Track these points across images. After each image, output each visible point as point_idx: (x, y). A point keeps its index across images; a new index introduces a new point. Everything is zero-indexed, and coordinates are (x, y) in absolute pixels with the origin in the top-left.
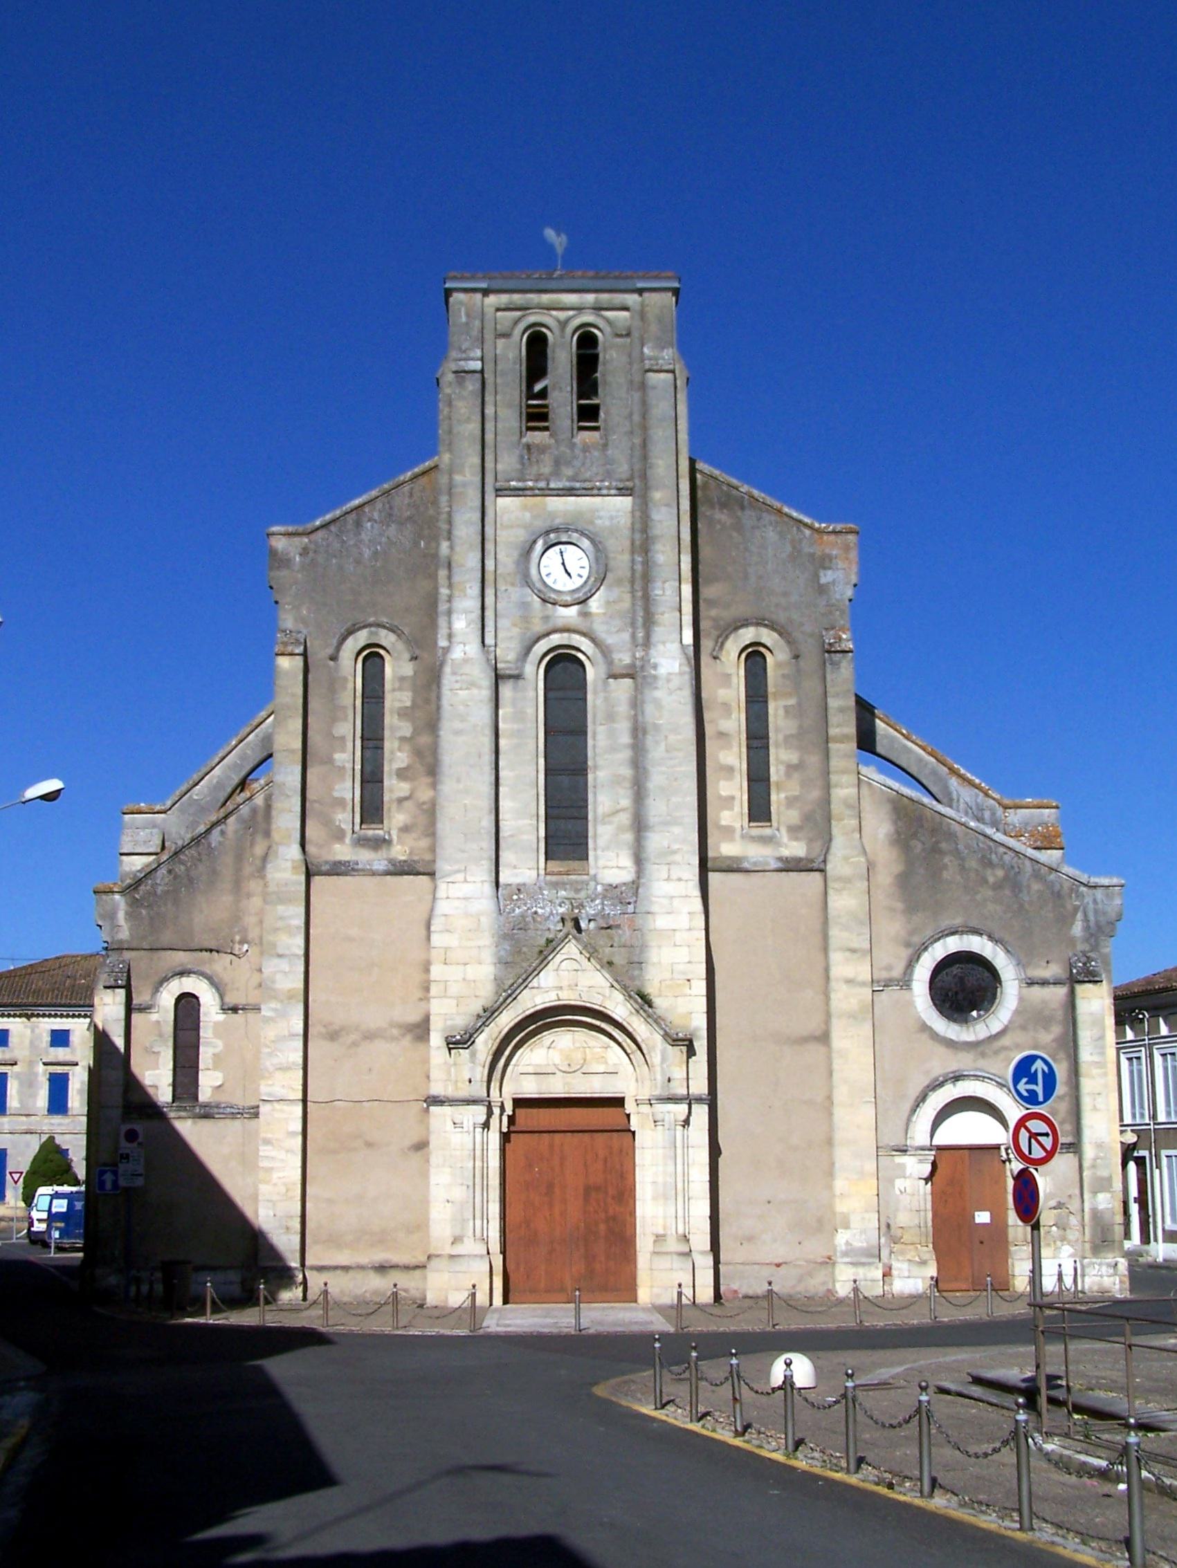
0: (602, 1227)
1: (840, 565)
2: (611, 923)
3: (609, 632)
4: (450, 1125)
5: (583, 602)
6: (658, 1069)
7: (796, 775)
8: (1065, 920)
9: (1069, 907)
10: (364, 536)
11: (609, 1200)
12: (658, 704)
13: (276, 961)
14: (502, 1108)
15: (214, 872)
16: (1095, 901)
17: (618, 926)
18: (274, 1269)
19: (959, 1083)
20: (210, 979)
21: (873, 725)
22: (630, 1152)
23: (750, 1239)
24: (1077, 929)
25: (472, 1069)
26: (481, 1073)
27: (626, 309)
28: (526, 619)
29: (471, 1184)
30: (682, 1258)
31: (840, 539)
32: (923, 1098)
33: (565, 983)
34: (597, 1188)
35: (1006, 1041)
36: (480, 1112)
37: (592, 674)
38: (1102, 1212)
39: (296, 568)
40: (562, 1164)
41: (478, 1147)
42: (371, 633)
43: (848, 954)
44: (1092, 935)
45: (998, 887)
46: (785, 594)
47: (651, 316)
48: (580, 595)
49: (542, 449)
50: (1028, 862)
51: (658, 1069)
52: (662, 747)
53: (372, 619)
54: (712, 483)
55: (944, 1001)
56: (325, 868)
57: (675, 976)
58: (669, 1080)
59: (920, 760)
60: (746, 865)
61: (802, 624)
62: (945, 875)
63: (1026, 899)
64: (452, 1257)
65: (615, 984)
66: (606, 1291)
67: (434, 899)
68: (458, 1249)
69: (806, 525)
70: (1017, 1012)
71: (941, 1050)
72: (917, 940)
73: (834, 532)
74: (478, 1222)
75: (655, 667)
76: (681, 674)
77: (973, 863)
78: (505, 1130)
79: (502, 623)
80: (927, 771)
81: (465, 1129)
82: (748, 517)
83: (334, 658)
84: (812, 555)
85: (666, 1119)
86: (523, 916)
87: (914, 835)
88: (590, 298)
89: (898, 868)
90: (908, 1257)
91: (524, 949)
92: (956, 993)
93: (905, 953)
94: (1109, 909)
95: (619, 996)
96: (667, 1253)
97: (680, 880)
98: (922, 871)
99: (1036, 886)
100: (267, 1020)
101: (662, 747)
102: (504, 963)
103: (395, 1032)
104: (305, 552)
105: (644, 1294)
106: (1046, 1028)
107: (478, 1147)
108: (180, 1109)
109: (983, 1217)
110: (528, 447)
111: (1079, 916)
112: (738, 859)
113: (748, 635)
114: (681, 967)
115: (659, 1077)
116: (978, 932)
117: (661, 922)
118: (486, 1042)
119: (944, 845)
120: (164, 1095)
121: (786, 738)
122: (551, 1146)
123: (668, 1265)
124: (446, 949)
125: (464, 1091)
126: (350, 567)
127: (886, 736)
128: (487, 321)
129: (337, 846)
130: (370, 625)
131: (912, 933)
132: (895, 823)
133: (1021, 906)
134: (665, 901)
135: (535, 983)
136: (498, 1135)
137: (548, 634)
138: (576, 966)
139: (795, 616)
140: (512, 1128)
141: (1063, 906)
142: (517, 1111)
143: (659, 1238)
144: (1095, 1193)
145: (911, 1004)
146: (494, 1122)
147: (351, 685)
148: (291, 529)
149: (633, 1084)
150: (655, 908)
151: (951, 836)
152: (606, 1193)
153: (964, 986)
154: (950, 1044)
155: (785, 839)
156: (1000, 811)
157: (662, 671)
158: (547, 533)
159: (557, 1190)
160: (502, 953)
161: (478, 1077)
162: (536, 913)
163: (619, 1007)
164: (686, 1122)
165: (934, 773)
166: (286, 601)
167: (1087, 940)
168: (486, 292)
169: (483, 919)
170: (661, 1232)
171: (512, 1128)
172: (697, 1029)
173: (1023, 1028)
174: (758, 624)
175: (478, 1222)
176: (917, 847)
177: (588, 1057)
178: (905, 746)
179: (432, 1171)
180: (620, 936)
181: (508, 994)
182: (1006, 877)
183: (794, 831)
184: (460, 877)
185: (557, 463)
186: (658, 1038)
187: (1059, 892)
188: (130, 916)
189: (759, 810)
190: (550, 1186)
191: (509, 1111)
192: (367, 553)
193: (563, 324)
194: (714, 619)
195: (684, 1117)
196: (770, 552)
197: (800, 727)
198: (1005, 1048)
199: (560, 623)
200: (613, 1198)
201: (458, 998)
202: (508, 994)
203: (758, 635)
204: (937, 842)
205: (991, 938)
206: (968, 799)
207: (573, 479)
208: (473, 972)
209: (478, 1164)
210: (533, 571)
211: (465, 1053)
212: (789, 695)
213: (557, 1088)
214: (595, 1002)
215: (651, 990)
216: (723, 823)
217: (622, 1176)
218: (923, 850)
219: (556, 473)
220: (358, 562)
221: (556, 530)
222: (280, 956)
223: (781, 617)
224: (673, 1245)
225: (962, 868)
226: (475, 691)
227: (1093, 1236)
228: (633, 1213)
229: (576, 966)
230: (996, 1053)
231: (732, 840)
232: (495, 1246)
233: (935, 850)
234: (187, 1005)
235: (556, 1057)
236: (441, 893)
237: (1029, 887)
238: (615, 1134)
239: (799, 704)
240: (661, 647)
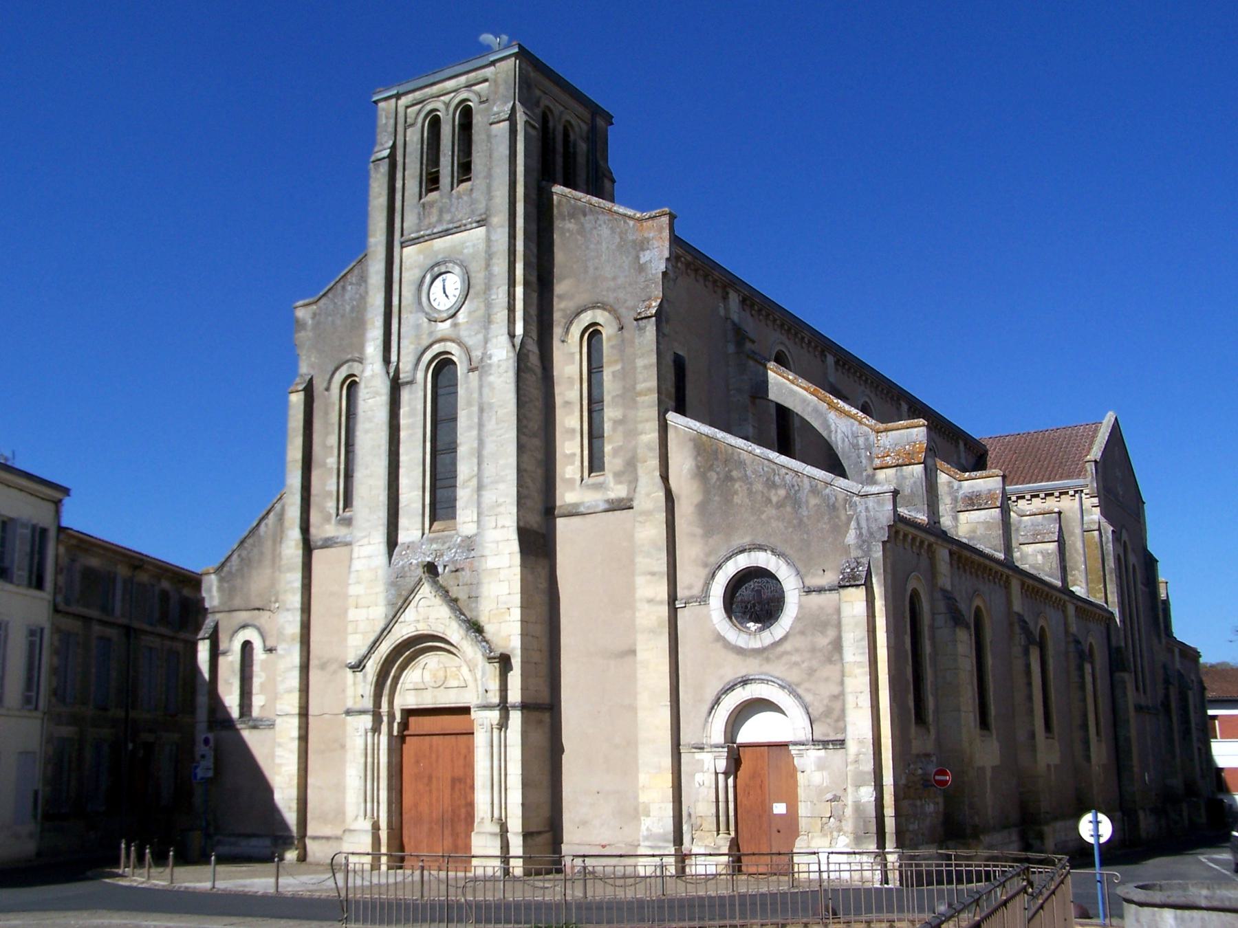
1: (656, 244)
3: (470, 336)
5: (454, 315)
7: (621, 428)
8: (839, 530)
9: (843, 518)
10: (347, 296)
12: (492, 387)
13: (286, 614)
14: (391, 716)
15: (262, 553)
16: (867, 508)
18: (281, 837)
19: (748, 687)
20: (258, 629)
21: (766, 375)
23: (584, 823)
24: (851, 537)
27: (486, 80)
28: (418, 337)
31: (655, 223)
32: (717, 701)
33: (420, 618)
34: (460, 780)
35: (787, 646)
37: (461, 369)
38: (863, 804)
39: (309, 328)
42: (350, 367)
43: (649, 577)
44: (864, 542)
45: (780, 505)
46: (614, 278)
47: (500, 81)
48: (452, 311)
49: (432, 204)
50: (806, 480)
52: (493, 421)
53: (349, 357)
54: (564, 200)
55: (744, 613)
56: (320, 543)
59: (804, 400)
60: (582, 509)
61: (626, 301)
62: (737, 499)
63: (805, 513)
67: (351, 559)
69: (630, 217)
70: (797, 619)
71: (732, 657)
72: (713, 560)
73: (650, 218)
75: (490, 358)
76: (507, 359)
77: (758, 487)
79: (404, 343)
80: (810, 409)
82: (588, 221)
83: (327, 389)
84: (634, 241)
86: (403, 567)
87: (711, 468)
88: (463, 79)
89: (697, 498)
90: (706, 842)
92: (754, 605)
93: (704, 573)
94: (879, 515)
97: (503, 527)
98: (717, 498)
99: (813, 501)
100: (283, 657)
101: (493, 421)
102: (391, 604)
104: (314, 315)
106: (823, 633)
108: (244, 722)
109: (779, 808)
110: (424, 206)
111: (853, 524)
112: (576, 505)
113: (586, 318)
116: (760, 548)
117: (490, 563)
119: (734, 473)
120: (235, 713)
121: (613, 398)
122: (431, 746)
124: (358, 596)
126: (338, 322)
127: (777, 384)
128: (400, 113)
129: (327, 527)
130: (347, 361)
131: (708, 555)
132: (696, 458)
133: (801, 521)
134: (493, 546)
137: (431, 345)
139: (621, 295)
141: (838, 517)
144: (858, 786)
145: (709, 617)
147: (337, 407)
148: (306, 301)
150: (487, 552)
151: (741, 464)
153: (753, 599)
154: (740, 651)
155: (612, 484)
156: (872, 436)
157: (495, 360)
158: (432, 268)
165: (816, 410)
166: (303, 354)
167: (860, 547)
168: (398, 96)
172: (514, 649)
173: (802, 633)
174: (593, 308)
176: (713, 476)
178: (792, 391)
182: (787, 496)
183: (618, 475)
184: (365, 541)
185: (441, 212)
187: (834, 505)
188: (220, 589)
189: (595, 463)
190: (430, 778)
192: (348, 308)
193: (447, 105)
194: (563, 310)
196: (604, 245)
197: (624, 387)
198: (786, 653)
199: (439, 335)
203: (594, 317)
204: (730, 471)
205: (773, 552)
206: (844, 429)
207: (451, 222)
210: (424, 299)
212: (616, 362)
213: (428, 701)
214: (438, 630)
215: (483, 620)
216: (567, 476)
218: (718, 479)
219: (440, 221)
220: (343, 316)
221: (438, 264)
222: (288, 610)
223: (610, 298)
225: (750, 492)
226: (378, 398)
227: (856, 827)
229: (428, 603)
230: (779, 657)
231: (573, 489)
233: (729, 478)
234: (247, 646)
236: (355, 555)
237: (807, 501)
239: (623, 368)
240: (494, 340)
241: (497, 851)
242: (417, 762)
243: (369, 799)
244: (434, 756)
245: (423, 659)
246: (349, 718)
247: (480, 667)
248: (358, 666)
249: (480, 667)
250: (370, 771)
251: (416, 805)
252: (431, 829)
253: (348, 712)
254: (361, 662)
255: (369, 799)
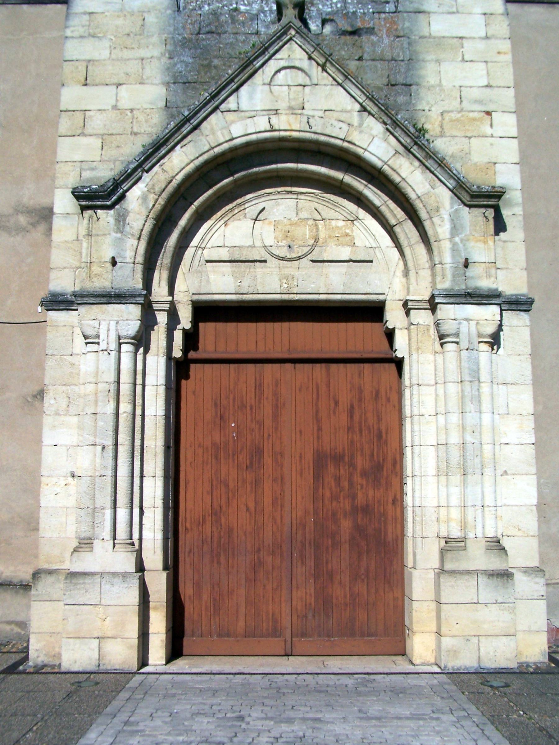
0: (346, 524)
2: (359, 24)
4: (79, 340)
6: (446, 245)
11: (358, 479)
14: (173, 317)
17: (371, 31)
22: (394, 397)
25: (118, 243)
26: (133, 249)
29: (109, 442)
30: (495, 581)
34: (338, 459)
36: (129, 317)
40: (276, 417)
41: (126, 378)
51: (446, 245)
57: (465, 104)
58: (466, 265)
64: (72, 575)
65: (370, 106)
66: (352, 634)
68: (86, 562)
74: (122, 513)
78: (177, 353)
81: (103, 346)
85: (464, 329)
86: (215, 14)
91: (216, 62)
95: (375, 127)
96: (468, 572)
102: (178, 81)
103: (22, 219)
105: (422, 647)
107: (126, 378)
114: (476, 93)
115: (447, 258)
118: (144, 198)
122: (259, 387)
123: (471, 596)
125: (103, 281)
135: (231, 103)
136: (162, 360)
138: (301, 78)
140: (192, 355)
142: (201, 325)
143: (451, 545)
146: (158, 338)
149: (398, 281)
152: (352, 465)
159: (268, 460)
160: (180, 67)
161: (129, 255)
162: (236, 10)
163: (375, 144)
164: (495, 341)
169: (151, 19)
170: (456, 533)
171: (192, 355)
175: (122, 513)
177: (322, 234)
179: (47, 420)
180: (373, 44)
181: (183, 125)
186: (444, 195)
190: (257, 453)
191: (186, 322)
195: (491, 329)
200: (364, 474)
201: (105, 138)
202: (183, 125)
208: (127, 96)
209: (125, 407)
211: (107, 217)
213: (269, 284)
217: (380, 437)
224: (478, 558)
228: (398, 500)
232: (154, 557)
235: (267, 235)
238: (367, 366)
241: (132, 568)
242: (222, 419)
243: (122, 499)
244: (267, 409)
245: (253, 202)
246: (53, 315)
247: (445, 213)
248: (97, 198)
249: (445, 213)
250: (126, 432)
251: (216, 514)
252: (257, 566)
253: (58, 302)
254: (117, 184)
255: (122, 499)
